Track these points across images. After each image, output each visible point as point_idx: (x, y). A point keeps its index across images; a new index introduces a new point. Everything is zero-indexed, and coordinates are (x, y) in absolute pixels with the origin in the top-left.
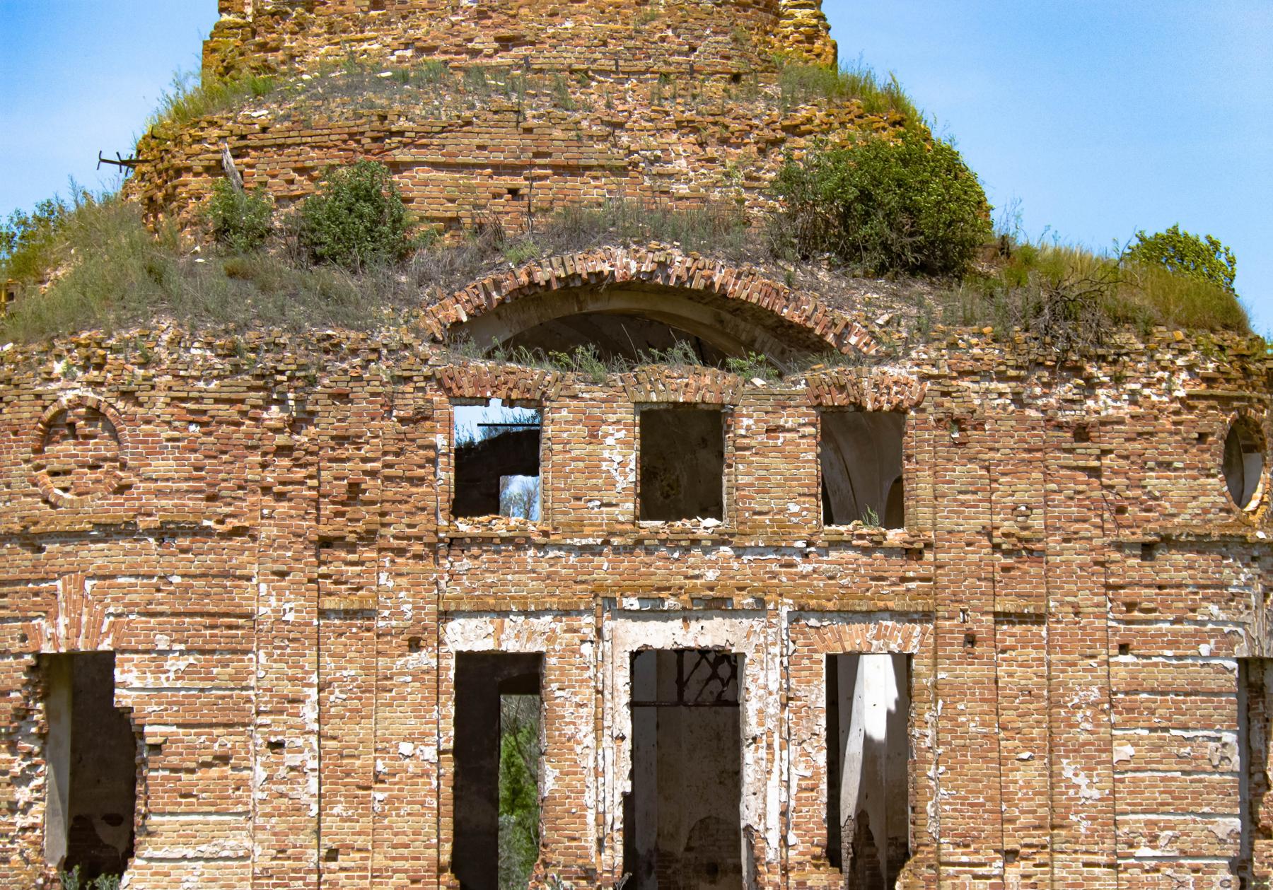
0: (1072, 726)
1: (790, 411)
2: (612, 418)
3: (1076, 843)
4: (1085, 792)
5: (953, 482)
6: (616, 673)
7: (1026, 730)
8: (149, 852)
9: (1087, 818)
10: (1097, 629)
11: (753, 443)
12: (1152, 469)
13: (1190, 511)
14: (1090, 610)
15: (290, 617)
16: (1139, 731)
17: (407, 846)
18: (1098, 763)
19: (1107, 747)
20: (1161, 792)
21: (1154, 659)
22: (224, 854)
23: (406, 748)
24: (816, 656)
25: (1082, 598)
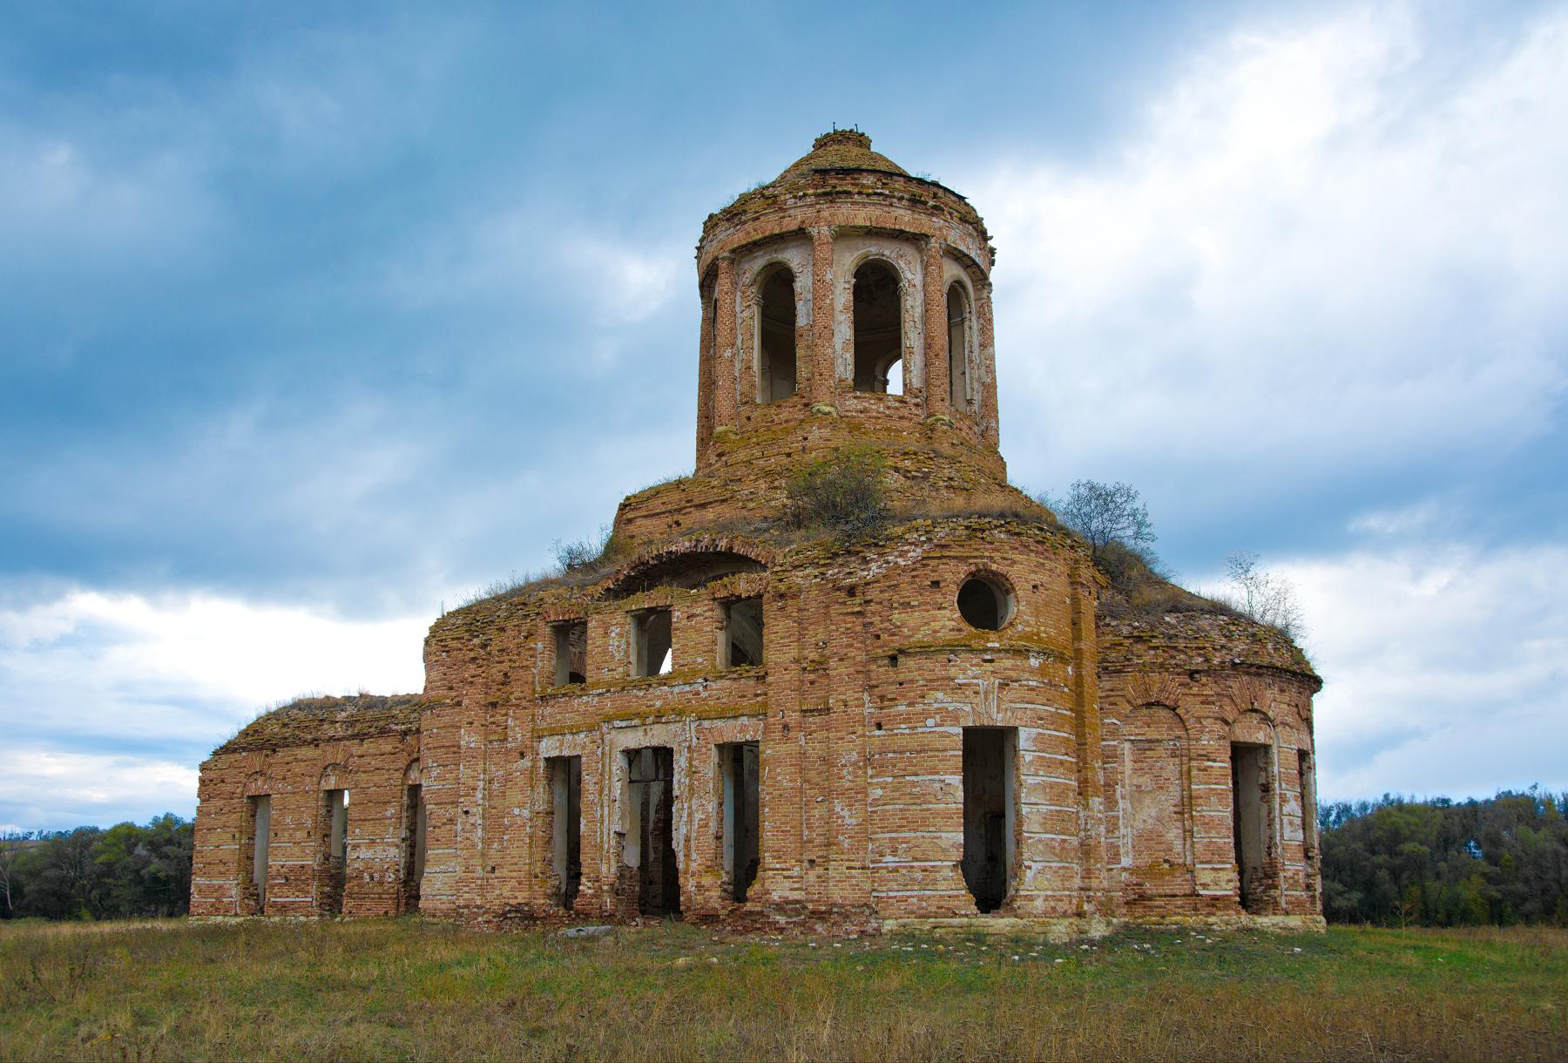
0: (841, 778)
1: (699, 604)
2: (614, 622)
3: (843, 853)
4: (848, 821)
5: (777, 632)
6: (612, 764)
7: (821, 783)
8: (428, 870)
9: (849, 837)
10: (857, 714)
11: (680, 625)
12: (896, 608)
13: (923, 633)
14: (852, 703)
15: (473, 745)
16: (886, 779)
17: (516, 864)
18: (856, 801)
19: (864, 791)
20: (899, 819)
21: (895, 731)
22: (450, 870)
23: (517, 811)
24: (709, 746)
25: (850, 696)
